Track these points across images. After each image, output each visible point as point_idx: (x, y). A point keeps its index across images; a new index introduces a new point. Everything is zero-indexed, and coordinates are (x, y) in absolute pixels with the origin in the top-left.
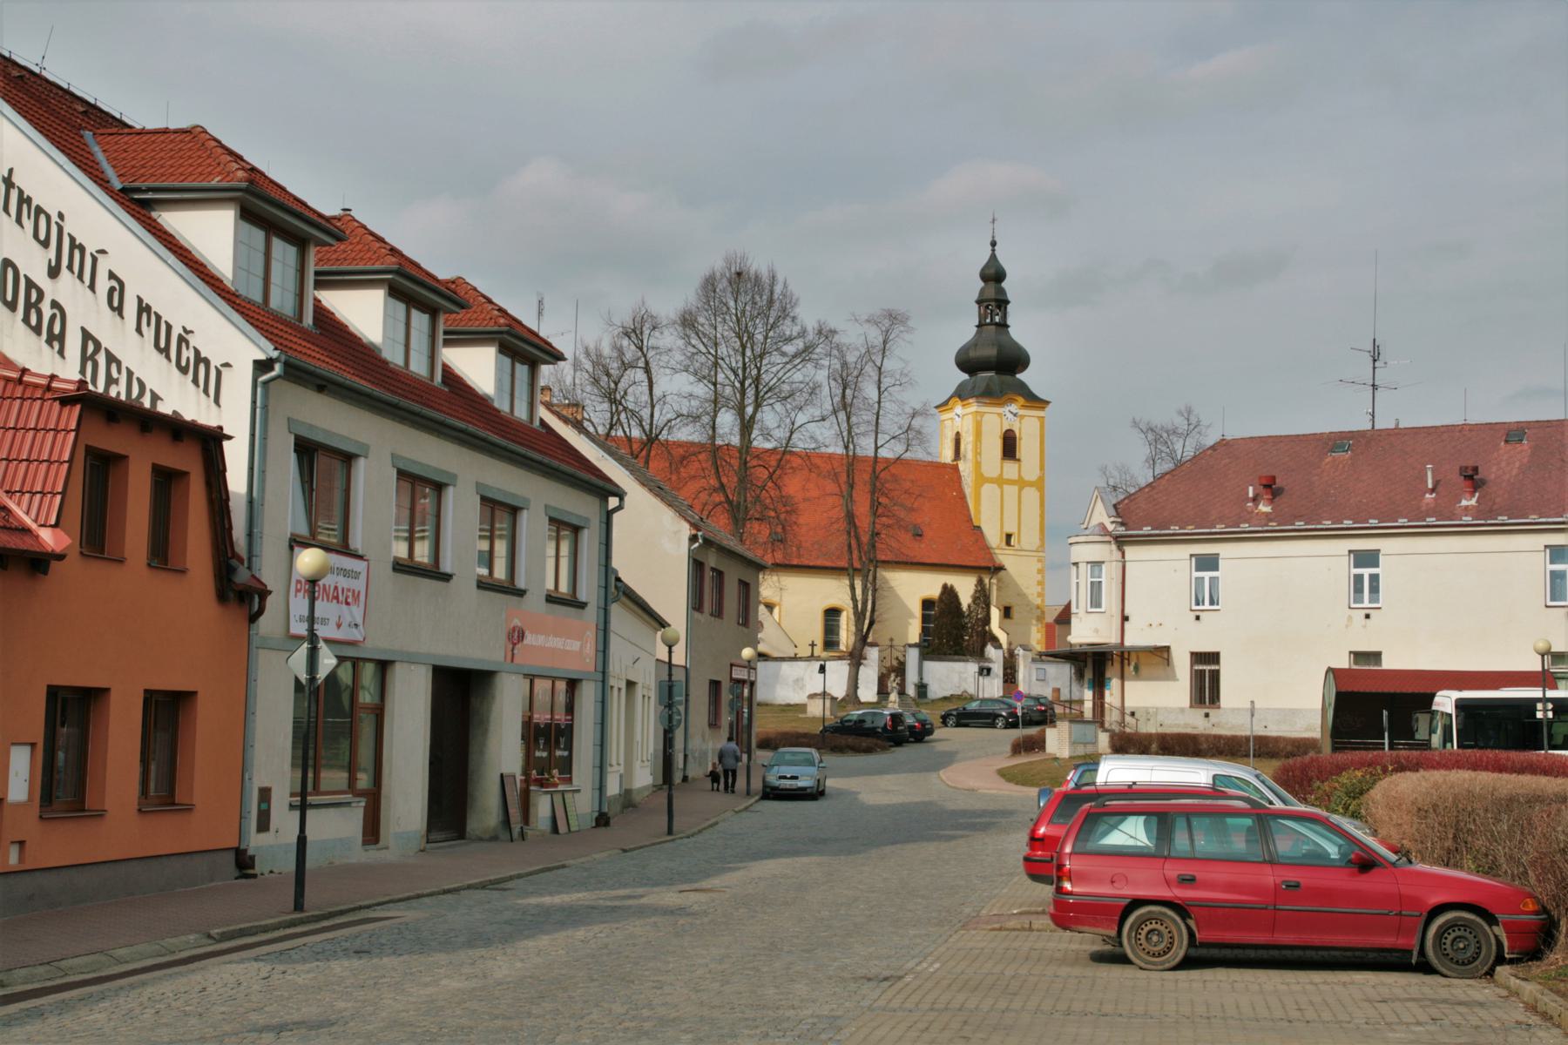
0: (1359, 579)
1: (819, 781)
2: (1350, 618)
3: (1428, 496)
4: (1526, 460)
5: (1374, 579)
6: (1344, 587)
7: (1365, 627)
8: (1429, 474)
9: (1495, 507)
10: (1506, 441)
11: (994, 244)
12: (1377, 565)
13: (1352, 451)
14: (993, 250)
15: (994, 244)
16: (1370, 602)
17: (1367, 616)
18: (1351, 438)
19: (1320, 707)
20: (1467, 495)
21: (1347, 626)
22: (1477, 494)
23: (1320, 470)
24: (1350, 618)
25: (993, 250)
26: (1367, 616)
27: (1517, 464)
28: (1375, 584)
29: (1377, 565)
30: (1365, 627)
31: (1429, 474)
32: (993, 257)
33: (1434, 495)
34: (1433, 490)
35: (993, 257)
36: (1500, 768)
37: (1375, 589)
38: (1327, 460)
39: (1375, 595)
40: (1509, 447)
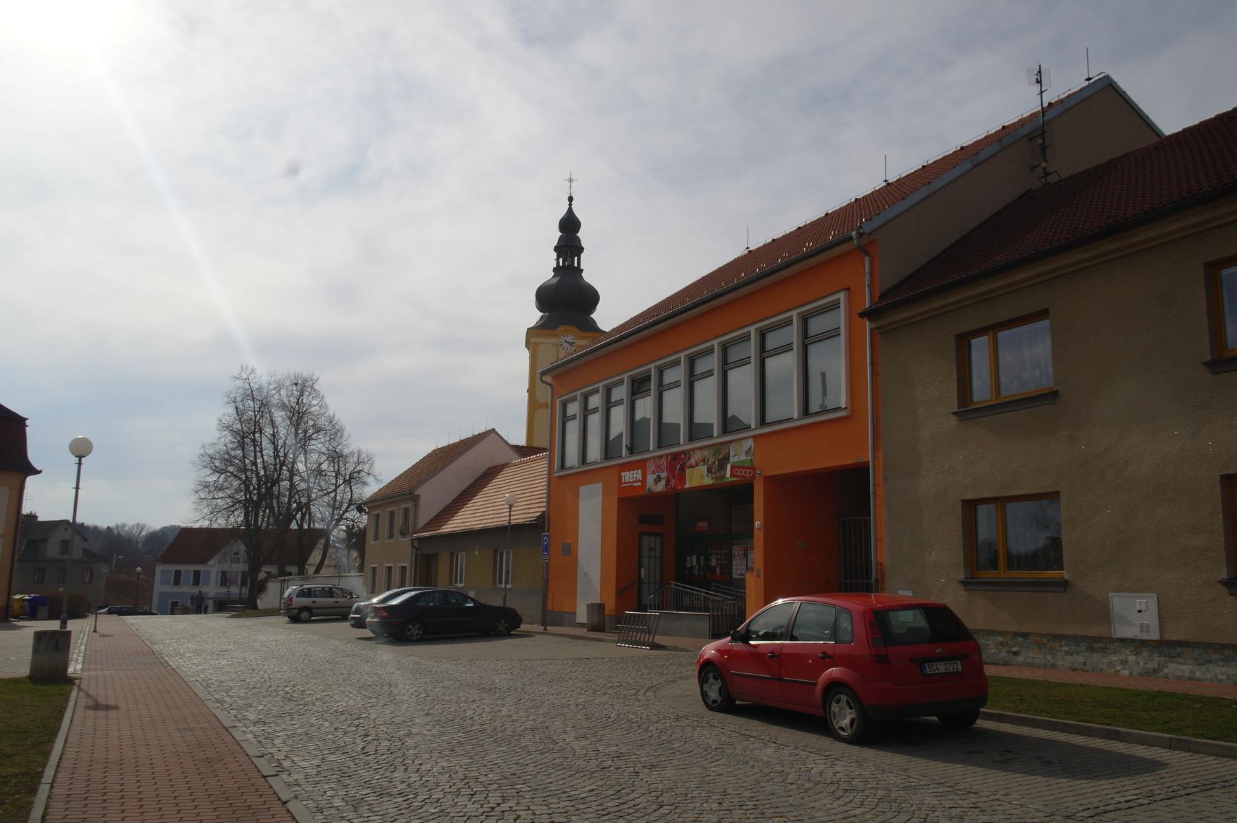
11: (571, 199)
14: (570, 205)
15: (571, 199)
25: (570, 205)
32: (570, 211)
35: (570, 211)
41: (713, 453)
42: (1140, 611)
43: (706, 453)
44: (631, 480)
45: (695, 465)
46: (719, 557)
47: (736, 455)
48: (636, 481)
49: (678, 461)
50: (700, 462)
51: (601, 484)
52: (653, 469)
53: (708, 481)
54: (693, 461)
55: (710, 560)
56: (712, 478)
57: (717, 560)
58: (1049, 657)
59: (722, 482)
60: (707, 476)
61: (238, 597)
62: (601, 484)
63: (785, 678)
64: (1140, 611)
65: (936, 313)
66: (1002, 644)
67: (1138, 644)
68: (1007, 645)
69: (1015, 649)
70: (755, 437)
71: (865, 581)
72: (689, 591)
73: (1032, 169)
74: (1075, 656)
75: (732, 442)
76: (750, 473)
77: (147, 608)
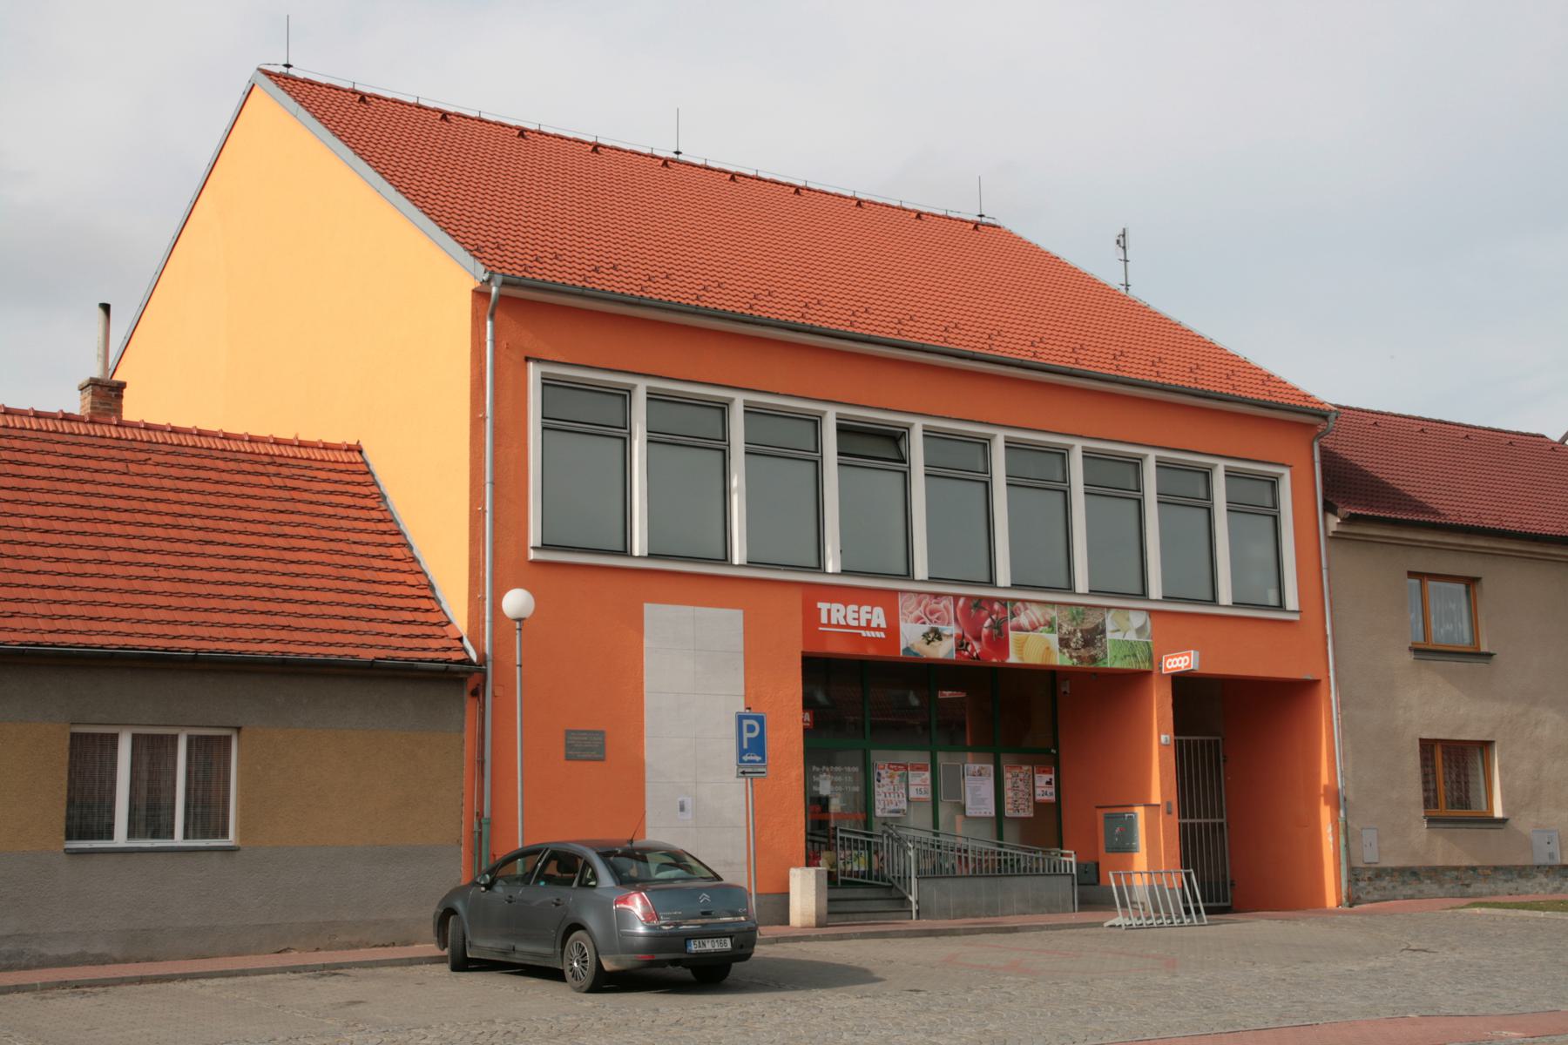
41: (1070, 617)
42: (1549, 843)
43: (1053, 613)
44: (855, 623)
45: (1029, 628)
46: (839, 779)
47: (1118, 630)
48: (868, 627)
49: (985, 613)
50: (1041, 625)
51: (647, 606)
52: (917, 613)
53: (1061, 659)
54: (1023, 620)
55: (817, 784)
56: (1071, 657)
57: (833, 784)
58: (1493, 886)
59: (1092, 666)
60: (1060, 651)
61: (875, 755)
62: (647, 606)
63: (605, 986)
64: (1549, 843)
65: (1469, 549)
66: (1457, 878)
67: (1547, 869)
68: (1460, 879)
69: (1467, 882)
70: (1151, 612)
71: (1188, 821)
72: (853, 837)
73: (106, 308)
74: (1510, 883)
75: (1109, 608)
76: (1186, 661)
77: (191, 832)
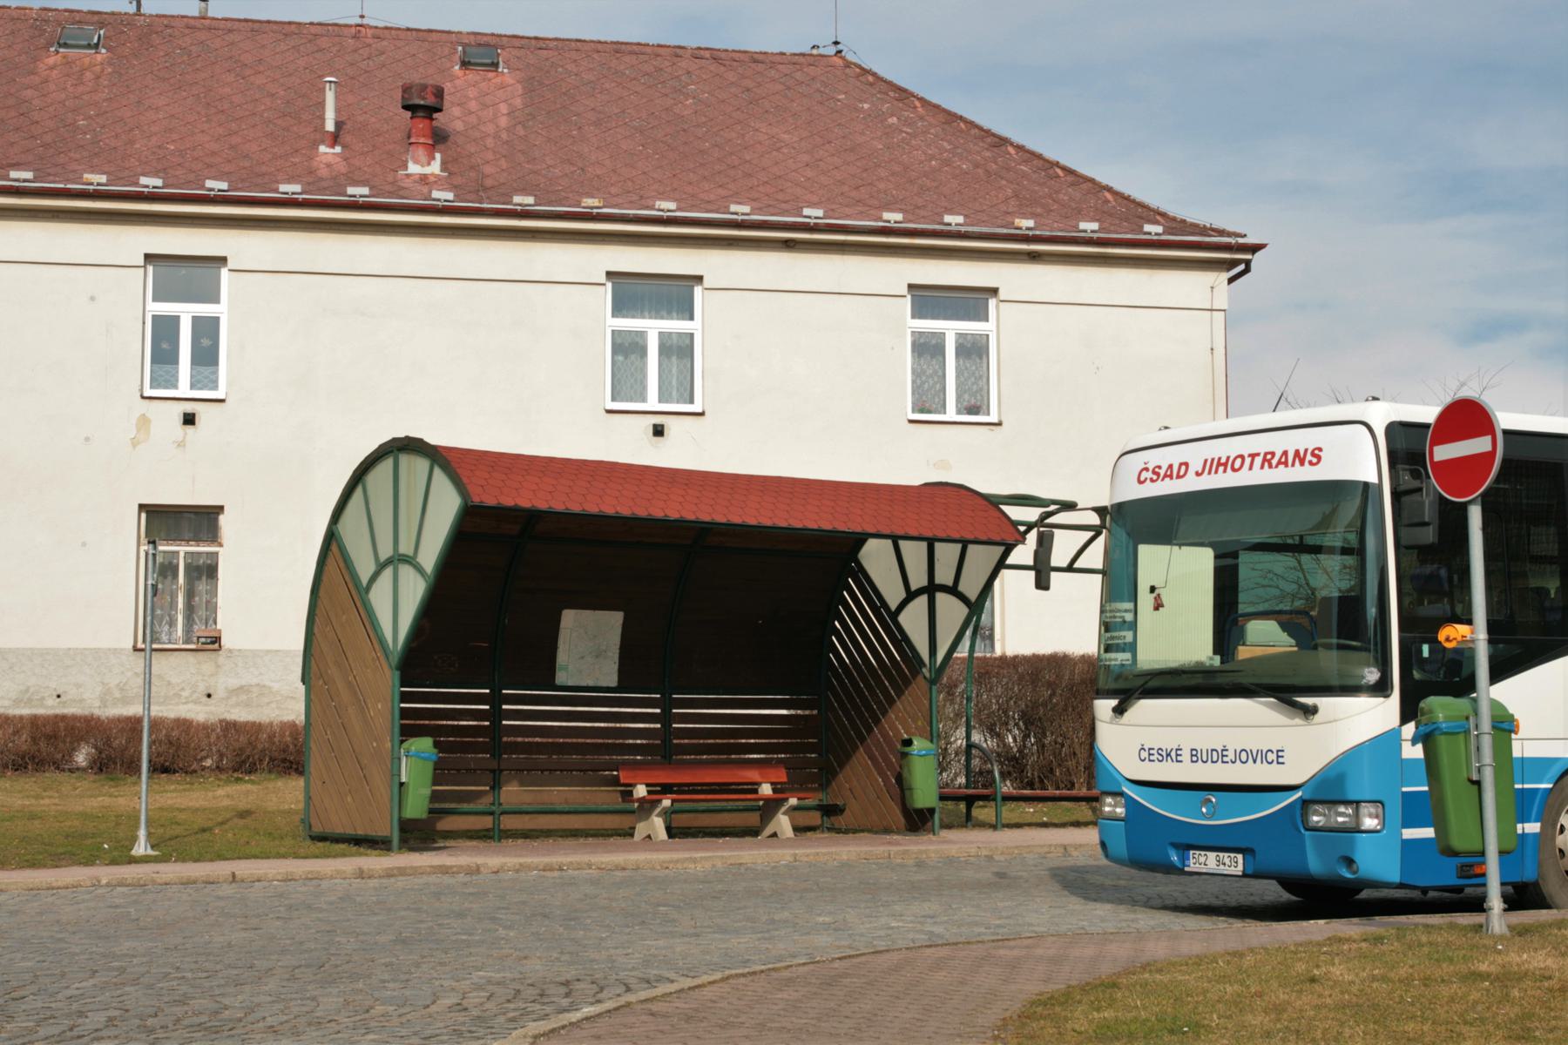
0: (165, 329)
1: (1245, 235)
2: (144, 422)
3: (323, 149)
4: (518, 102)
5: (207, 330)
6: (136, 345)
7: (181, 444)
8: (330, 97)
9: (684, 90)
10: (465, 64)
12: (214, 298)
13: (109, 49)
16: (193, 387)
17: (189, 420)
18: (102, 25)
19: (301, 646)
20: (421, 152)
21: (135, 443)
22: (438, 156)
23: (37, 79)
24: (144, 422)
26: (189, 420)
27: (504, 108)
28: (206, 342)
29: (214, 298)
30: (181, 444)
31: (330, 97)
33: (338, 149)
34: (335, 139)
36: (890, 843)
37: (206, 356)
38: (51, 61)
39: (206, 370)
40: (471, 76)
